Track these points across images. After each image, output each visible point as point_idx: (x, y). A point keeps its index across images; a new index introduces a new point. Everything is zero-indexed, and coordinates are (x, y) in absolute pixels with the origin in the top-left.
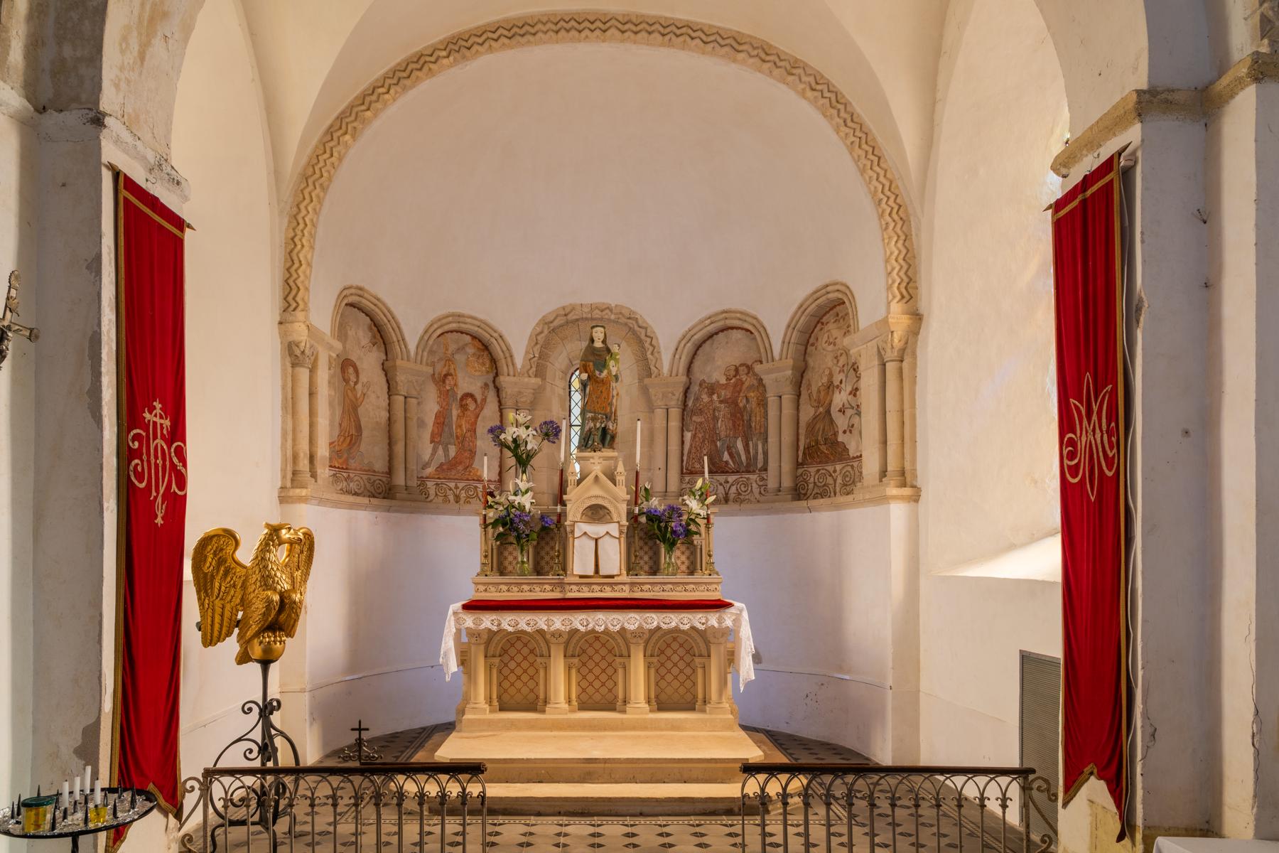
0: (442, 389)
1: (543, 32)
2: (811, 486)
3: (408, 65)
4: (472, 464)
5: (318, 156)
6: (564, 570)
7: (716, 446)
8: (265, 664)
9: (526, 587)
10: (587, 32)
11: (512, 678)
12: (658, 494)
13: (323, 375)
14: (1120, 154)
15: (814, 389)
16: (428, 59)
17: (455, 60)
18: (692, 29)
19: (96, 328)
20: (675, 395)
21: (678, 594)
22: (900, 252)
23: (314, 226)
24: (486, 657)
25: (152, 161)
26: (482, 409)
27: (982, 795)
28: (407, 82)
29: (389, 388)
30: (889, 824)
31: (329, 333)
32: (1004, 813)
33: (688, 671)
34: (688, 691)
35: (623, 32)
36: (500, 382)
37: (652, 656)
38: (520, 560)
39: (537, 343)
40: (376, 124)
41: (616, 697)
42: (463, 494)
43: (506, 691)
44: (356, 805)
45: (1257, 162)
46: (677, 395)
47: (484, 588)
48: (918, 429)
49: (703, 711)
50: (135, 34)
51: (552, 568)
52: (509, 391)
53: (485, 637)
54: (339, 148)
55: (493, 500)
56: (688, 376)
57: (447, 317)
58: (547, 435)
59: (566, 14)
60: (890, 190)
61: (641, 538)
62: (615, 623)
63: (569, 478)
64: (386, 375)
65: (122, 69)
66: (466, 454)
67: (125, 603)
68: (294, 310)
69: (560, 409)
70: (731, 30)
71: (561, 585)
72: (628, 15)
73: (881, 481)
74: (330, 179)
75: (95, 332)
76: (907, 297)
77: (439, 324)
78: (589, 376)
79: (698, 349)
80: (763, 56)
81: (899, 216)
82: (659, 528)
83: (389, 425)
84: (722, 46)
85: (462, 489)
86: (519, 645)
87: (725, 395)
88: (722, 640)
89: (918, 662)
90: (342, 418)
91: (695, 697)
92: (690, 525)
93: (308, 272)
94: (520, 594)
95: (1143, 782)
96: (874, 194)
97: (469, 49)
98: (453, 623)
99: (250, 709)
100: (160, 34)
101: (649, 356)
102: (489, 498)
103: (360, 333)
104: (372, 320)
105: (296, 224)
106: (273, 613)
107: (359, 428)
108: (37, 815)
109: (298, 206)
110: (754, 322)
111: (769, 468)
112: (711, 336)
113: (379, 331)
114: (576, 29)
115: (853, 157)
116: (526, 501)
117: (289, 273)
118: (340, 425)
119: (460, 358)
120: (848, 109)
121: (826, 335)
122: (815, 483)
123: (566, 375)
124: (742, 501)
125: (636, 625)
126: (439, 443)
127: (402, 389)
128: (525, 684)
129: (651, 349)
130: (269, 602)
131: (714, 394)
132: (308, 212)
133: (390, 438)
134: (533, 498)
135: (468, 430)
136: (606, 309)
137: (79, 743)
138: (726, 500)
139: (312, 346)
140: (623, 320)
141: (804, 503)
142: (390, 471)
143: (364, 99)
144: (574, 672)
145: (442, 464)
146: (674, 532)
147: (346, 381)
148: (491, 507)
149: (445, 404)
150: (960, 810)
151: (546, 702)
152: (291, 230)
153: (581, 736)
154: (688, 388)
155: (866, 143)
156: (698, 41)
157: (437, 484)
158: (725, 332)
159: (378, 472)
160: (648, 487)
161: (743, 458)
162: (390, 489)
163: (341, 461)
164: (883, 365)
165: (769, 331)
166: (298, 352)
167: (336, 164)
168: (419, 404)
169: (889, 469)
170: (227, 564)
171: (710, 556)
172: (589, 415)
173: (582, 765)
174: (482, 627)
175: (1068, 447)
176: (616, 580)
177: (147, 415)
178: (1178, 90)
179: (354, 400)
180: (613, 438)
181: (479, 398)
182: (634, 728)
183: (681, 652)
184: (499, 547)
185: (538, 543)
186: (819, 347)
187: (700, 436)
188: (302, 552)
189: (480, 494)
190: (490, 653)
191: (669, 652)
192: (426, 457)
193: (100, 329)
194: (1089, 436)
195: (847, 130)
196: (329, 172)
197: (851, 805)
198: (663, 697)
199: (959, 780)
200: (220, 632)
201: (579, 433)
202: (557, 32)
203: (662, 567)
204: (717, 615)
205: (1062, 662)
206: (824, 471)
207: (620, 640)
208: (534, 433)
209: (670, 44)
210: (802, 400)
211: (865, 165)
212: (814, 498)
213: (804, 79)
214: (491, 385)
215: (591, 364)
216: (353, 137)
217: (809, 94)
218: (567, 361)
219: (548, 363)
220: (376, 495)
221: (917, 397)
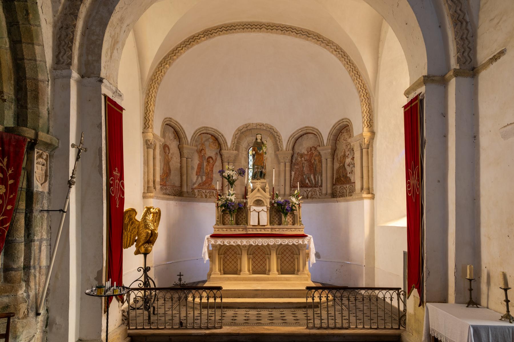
1: (238, 29)
2: (338, 193)
5: (156, 72)
6: (247, 223)
8: (145, 254)
9: (233, 230)
10: (254, 29)
11: (228, 262)
13: (158, 151)
15: (339, 157)
16: (197, 38)
17: (206, 38)
18: (292, 29)
19: (100, 146)
20: (288, 158)
21: (289, 232)
22: (367, 109)
24: (219, 254)
26: (215, 162)
27: (384, 296)
28: (189, 46)
29: (181, 155)
30: (369, 319)
31: (160, 136)
32: (391, 302)
33: (292, 260)
34: (292, 267)
35: (267, 29)
37: (279, 254)
38: (231, 219)
39: (236, 138)
40: (178, 60)
41: (266, 269)
42: (208, 195)
43: (226, 267)
44: (179, 300)
46: (289, 158)
47: (217, 230)
48: (374, 173)
49: (297, 274)
50: (109, 50)
51: (242, 222)
52: (225, 156)
54: (164, 69)
56: (293, 151)
57: (202, 128)
59: (247, 23)
60: (363, 87)
61: (275, 212)
63: (249, 190)
64: (179, 150)
65: (106, 62)
66: (209, 180)
68: (148, 128)
69: (245, 163)
70: (306, 29)
71: (246, 229)
72: (269, 23)
73: (361, 192)
74: (161, 81)
76: (370, 126)
77: (199, 131)
78: (255, 153)
79: (296, 141)
80: (318, 39)
82: (282, 208)
83: (181, 169)
85: (208, 193)
86: (230, 250)
87: (307, 158)
88: (304, 249)
90: (164, 167)
91: (294, 269)
93: (153, 114)
94: (231, 232)
95: (426, 288)
97: (212, 34)
98: (207, 242)
99: (140, 270)
100: (116, 48)
101: (278, 143)
102: (219, 197)
103: (170, 135)
104: (174, 130)
106: (149, 237)
107: (170, 170)
109: (149, 90)
110: (317, 131)
111: (323, 186)
112: (301, 136)
113: (177, 133)
114: (250, 28)
115: (350, 76)
116: (233, 198)
117: (146, 114)
118: (163, 169)
120: (348, 58)
121: (343, 137)
124: (313, 198)
125: (273, 243)
127: (186, 155)
129: (279, 140)
130: (148, 233)
131: (302, 157)
132: (153, 92)
134: (235, 197)
135: (210, 171)
136: (262, 125)
137: (96, 276)
138: (307, 197)
139: (154, 141)
140: (268, 129)
141: (335, 199)
142: (181, 186)
144: (251, 260)
145: (200, 183)
146: (287, 210)
147: (165, 153)
149: (201, 160)
154: (293, 155)
155: (355, 70)
156: (294, 33)
157: (198, 191)
158: (307, 134)
159: (177, 186)
160: (278, 193)
161: (314, 182)
162: (181, 193)
163: (163, 182)
164: (362, 150)
166: (149, 143)
167: (163, 75)
169: (364, 187)
170: (133, 220)
171: (300, 218)
172: (256, 167)
173: (254, 292)
174: (217, 243)
175: (408, 183)
176: (266, 227)
177: (114, 173)
178: (436, 76)
180: (264, 175)
181: (214, 158)
182: (272, 280)
183: (290, 253)
184: (223, 215)
185: (237, 213)
186: (341, 141)
187: (298, 173)
188: (157, 216)
189: (215, 195)
190: (220, 253)
191: (285, 253)
192: (194, 181)
194: (413, 182)
195: (348, 66)
196: (160, 78)
197: (342, 300)
198: (283, 269)
199: (377, 292)
201: (252, 171)
202: (243, 29)
203: (283, 222)
204: (302, 239)
205: (407, 253)
207: (267, 249)
208: (236, 173)
209: (284, 34)
210: (335, 161)
211: (354, 78)
212: (339, 197)
213: (333, 47)
214: (219, 153)
215: (256, 148)
216: (169, 65)
217: (334, 52)
218: (247, 144)
221: (373, 162)
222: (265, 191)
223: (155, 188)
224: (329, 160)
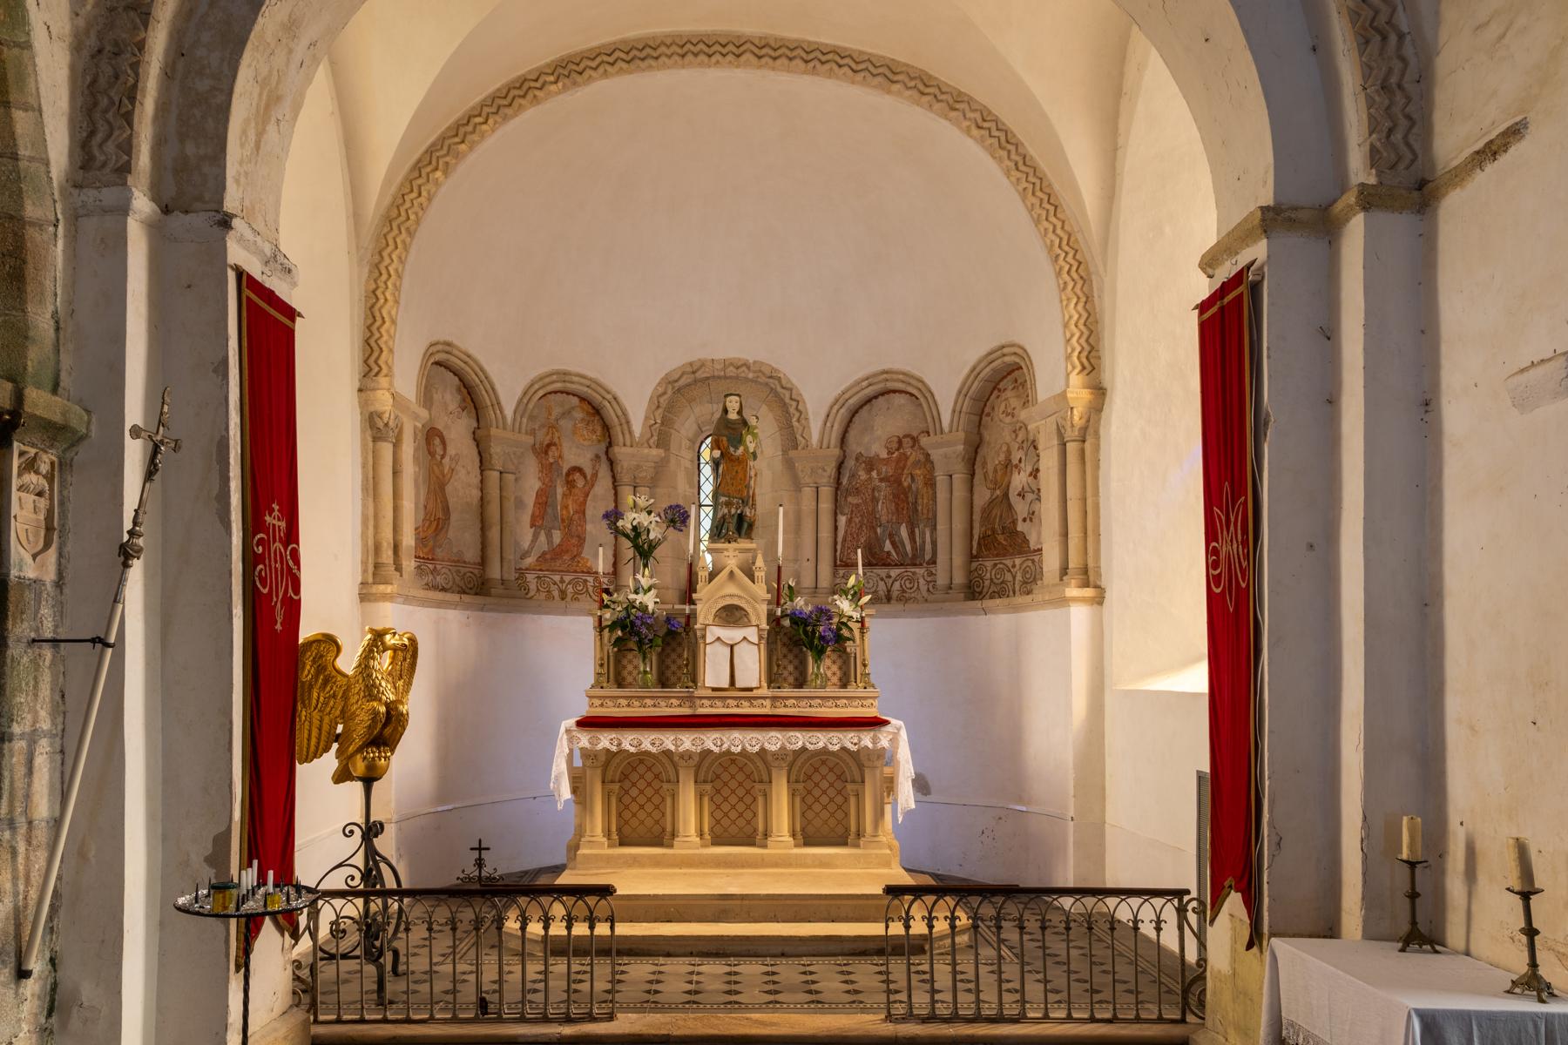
0: (544, 462)
1: (666, 55)
2: (987, 583)
3: (509, 91)
4: (581, 553)
5: (403, 195)
6: (694, 681)
7: (876, 533)
8: (368, 781)
9: (649, 702)
10: (718, 57)
12: (807, 591)
14: (1249, 269)
15: (990, 467)
16: (533, 84)
17: (564, 85)
19: (224, 433)
21: (828, 710)
22: (1080, 316)
23: (399, 277)
24: (603, 782)
25: (269, 254)
26: (593, 486)
27: (1136, 917)
28: (509, 111)
29: (481, 461)
30: (1087, 991)
31: (414, 400)
32: (1158, 936)
33: (839, 799)
34: (839, 822)
35: (760, 57)
36: (614, 454)
37: (797, 781)
38: (642, 669)
39: (658, 407)
41: (755, 830)
42: (570, 590)
43: (626, 822)
44: (477, 929)
45: (1366, 288)
46: (829, 470)
48: (1101, 521)
49: (857, 846)
50: (253, 125)
51: (679, 679)
52: (625, 464)
53: (603, 758)
54: (429, 186)
55: (610, 598)
56: (841, 448)
58: (673, 521)
60: (1068, 244)
62: (754, 743)
63: (700, 574)
64: (478, 446)
66: (574, 541)
67: (252, 711)
68: (376, 375)
69: (687, 486)
71: (691, 699)
72: (765, 38)
73: (1061, 580)
74: (418, 222)
75: (223, 437)
76: (1089, 368)
77: (541, 383)
78: (722, 453)
79: (853, 416)
80: (921, 87)
81: (1079, 274)
82: (805, 632)
84: (874, 76)
85: (569, 583)
86: (641, 769)
87: (886, 472)
88: (879, 763)
89: (1103, 789)
90: (427, 500)
91: (847, 830)
92: (841, 629)
93: (392, 331)
96: (1050, 248)
97: (581, 73)
98: (565, 742)
99: (352, 832)
100: (273, 119)
101: (795, 424)
102: (605, 596)
103: (449, 397)
104: (460, 380)
105: (377, 274)
106: (379, 726)
107: (446, 510)
108: (224, 897)
109: (380, 253)
110: (920, 385)
111: (938, 561)
112: (869, 401)
113: (469, 393)
114: (705, 53)
116: (649, 600)
118: (425, 507)
119: (566, 424)
120: (1020, 150)
121: (1003, 404)
122: (991, 579)
123: (694, 443)
124: (907, 600)
126: (540, 527)
127: (497, 463)
128: (649, 815)
129: (797, 415)
130: (376, 713)
131: (872, 470)
132: (392, 261)
133: (482, 521)
135: (576, 512)
136: (742, 365)
138: (889, 599)
139: (396, 417)
140: (763, 379)
141: (978, 604)
142: (483, 561)
143: (458, 129)
144: (706, 800)
145: (544, 553)
146: (822, 638)
147: (432, 454)
148: (607, 606)
150: (1112, 933)
151: (674, 835)
152: (372, 282)
153: (714, 874)
154: (842, 463)
155: (1041, 190)
156: (846, 69)
157: (539, 577)
158: (886, 396)
159: (469, 563)
160: (792, 584)
161: (908, 548)
163: (425, 550)
164: (1063, 445)
165: (937, 397)
166: (380, 424)
167: (424, 205)
168: (516, 480)
171: (865, 665)
172: (723, 499)
174: (600, 747)
175: (1211, 552)
176: (755, 693)
177: (267, 518)
178: (1302, 208)
179: (441, 477)
180: (751, 526)
181: (589, 472)
182: (776, 865)
183: (831, 777)
185: (663, 650)
186: (996, 419)
187: (857, 520)
188: (405, 659)
189: (591, 589)
190: (609, 777)
191: (816, 778)
192: (526, 544)
193: (228, 433)
195: (1019, 175)
196: (416, 214)
197: (999, 928)
199: (1112, 902)
200: (317, 748)
202: (683, 56)
203: (809, 679)
204: (872, 734)
206: (1001, 566)
207: (760, 764)
208: (658, 519)
209: (814, 71)
210: (977, 477)
212: (991, 598)
213: (970, 115)
214: (604, 458)
215: (725, 439)
217: (975, 132)
218: (695, 427)
219: (673, 431)
220: (467, 591)
222: (752, 577)
223: (398, 568)
224: (959, 479)
